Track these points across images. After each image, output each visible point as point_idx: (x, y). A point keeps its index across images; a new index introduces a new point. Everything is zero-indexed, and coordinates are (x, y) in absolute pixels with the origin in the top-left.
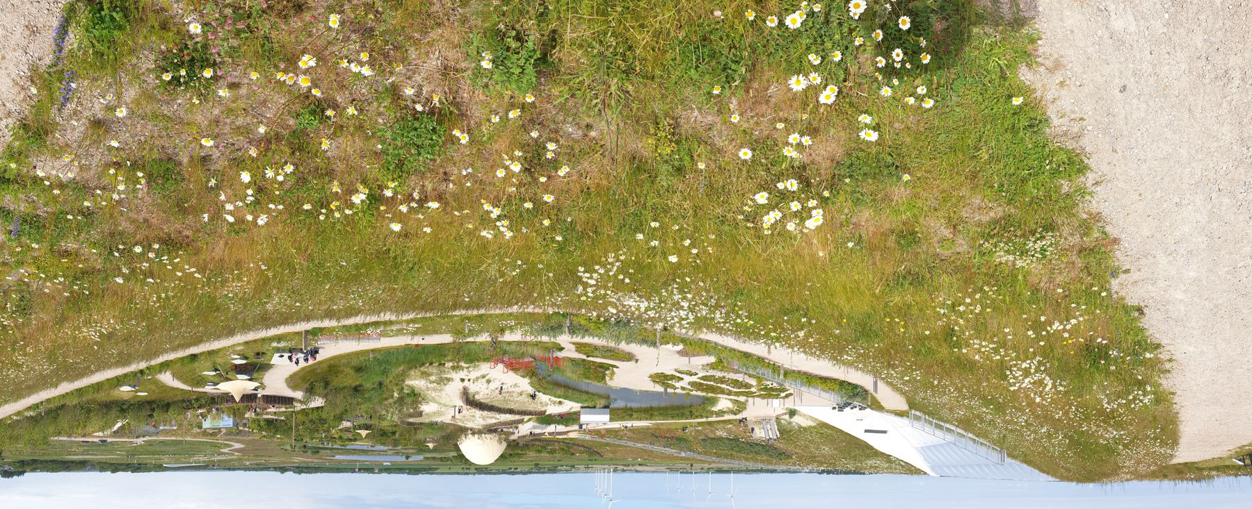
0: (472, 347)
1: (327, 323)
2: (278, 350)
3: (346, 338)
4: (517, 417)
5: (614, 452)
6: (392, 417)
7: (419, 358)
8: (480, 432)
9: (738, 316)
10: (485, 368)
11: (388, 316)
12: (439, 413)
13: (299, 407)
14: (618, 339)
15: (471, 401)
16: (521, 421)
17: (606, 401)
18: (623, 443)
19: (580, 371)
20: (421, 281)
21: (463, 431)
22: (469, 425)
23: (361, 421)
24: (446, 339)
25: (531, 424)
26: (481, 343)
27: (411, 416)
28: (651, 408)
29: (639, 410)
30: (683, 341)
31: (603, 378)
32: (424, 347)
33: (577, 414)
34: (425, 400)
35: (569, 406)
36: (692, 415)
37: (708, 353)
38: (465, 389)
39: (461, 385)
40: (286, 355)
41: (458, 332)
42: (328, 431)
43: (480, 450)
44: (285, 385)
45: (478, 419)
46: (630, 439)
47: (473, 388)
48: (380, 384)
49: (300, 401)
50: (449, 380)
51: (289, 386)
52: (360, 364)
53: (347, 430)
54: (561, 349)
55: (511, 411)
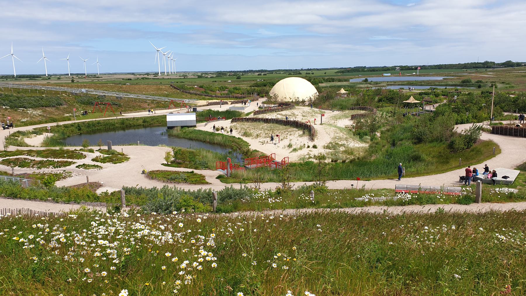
0: (306, 177)
1: (461, 208)
2: (508, 184)
3: (432, 191)
4: (260, 116)
5: (159, 89)
6: (382, 114)
7: (357, 167)
8: (297, 103)
9: (32, 242)
10: (294, 158)
11: (396, 211)
12: (336, 118)
13: (485, 125)
14: (165, 191)
15: (307, 129)
16: (256, 113)
17: (171, 133)
18: (151, 98)
19: (198, 159)
20: (370, 247)
21: (313, 104)
22: (307, 109)
23: (414, 111)
24: (332, 185)
25: (246, 111)
26: (299, 180)
27: (363, 116)
28: (123, 129)
29: (138, 126)
30: (97, 199)
31: (176, 154)
32: (351, 178)
33: (198, 121)
34: (348, 129)
35: (207, 127)
36: (79, 127)
37: (66, 191)
38: (312, 139)
39: (316, 142)
40: (499, 178)
41: (321, 191)
42: (450, 101)
43: (301, 89)
44: (502, 146)
45: (298, 114)
46: (145, 101)
47: (305, 140)
48: (394, 144)
49: (484, 130)
50: (328, 147)
51: (497, 146)
52: (415, 164)
53: (429, 103)
54: (219, 177)
55: (267, 121)
